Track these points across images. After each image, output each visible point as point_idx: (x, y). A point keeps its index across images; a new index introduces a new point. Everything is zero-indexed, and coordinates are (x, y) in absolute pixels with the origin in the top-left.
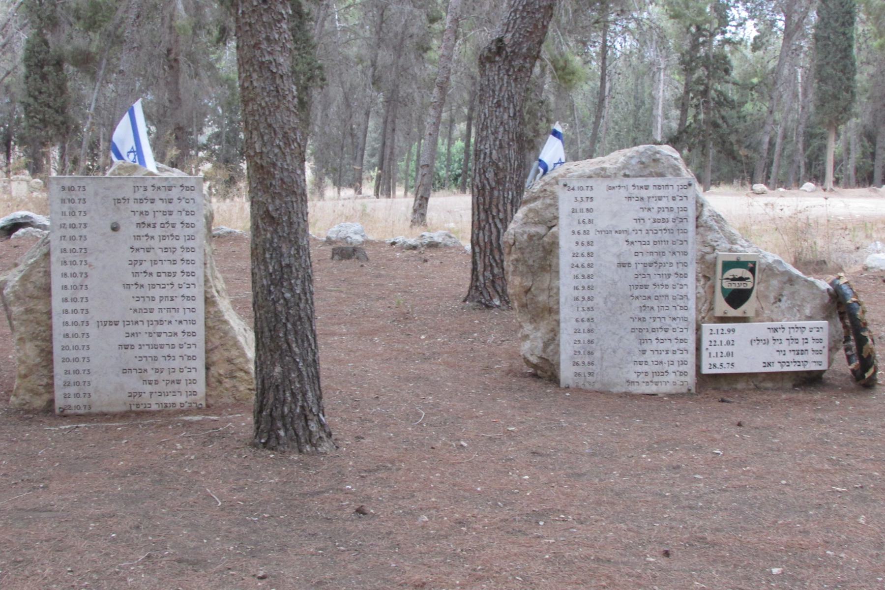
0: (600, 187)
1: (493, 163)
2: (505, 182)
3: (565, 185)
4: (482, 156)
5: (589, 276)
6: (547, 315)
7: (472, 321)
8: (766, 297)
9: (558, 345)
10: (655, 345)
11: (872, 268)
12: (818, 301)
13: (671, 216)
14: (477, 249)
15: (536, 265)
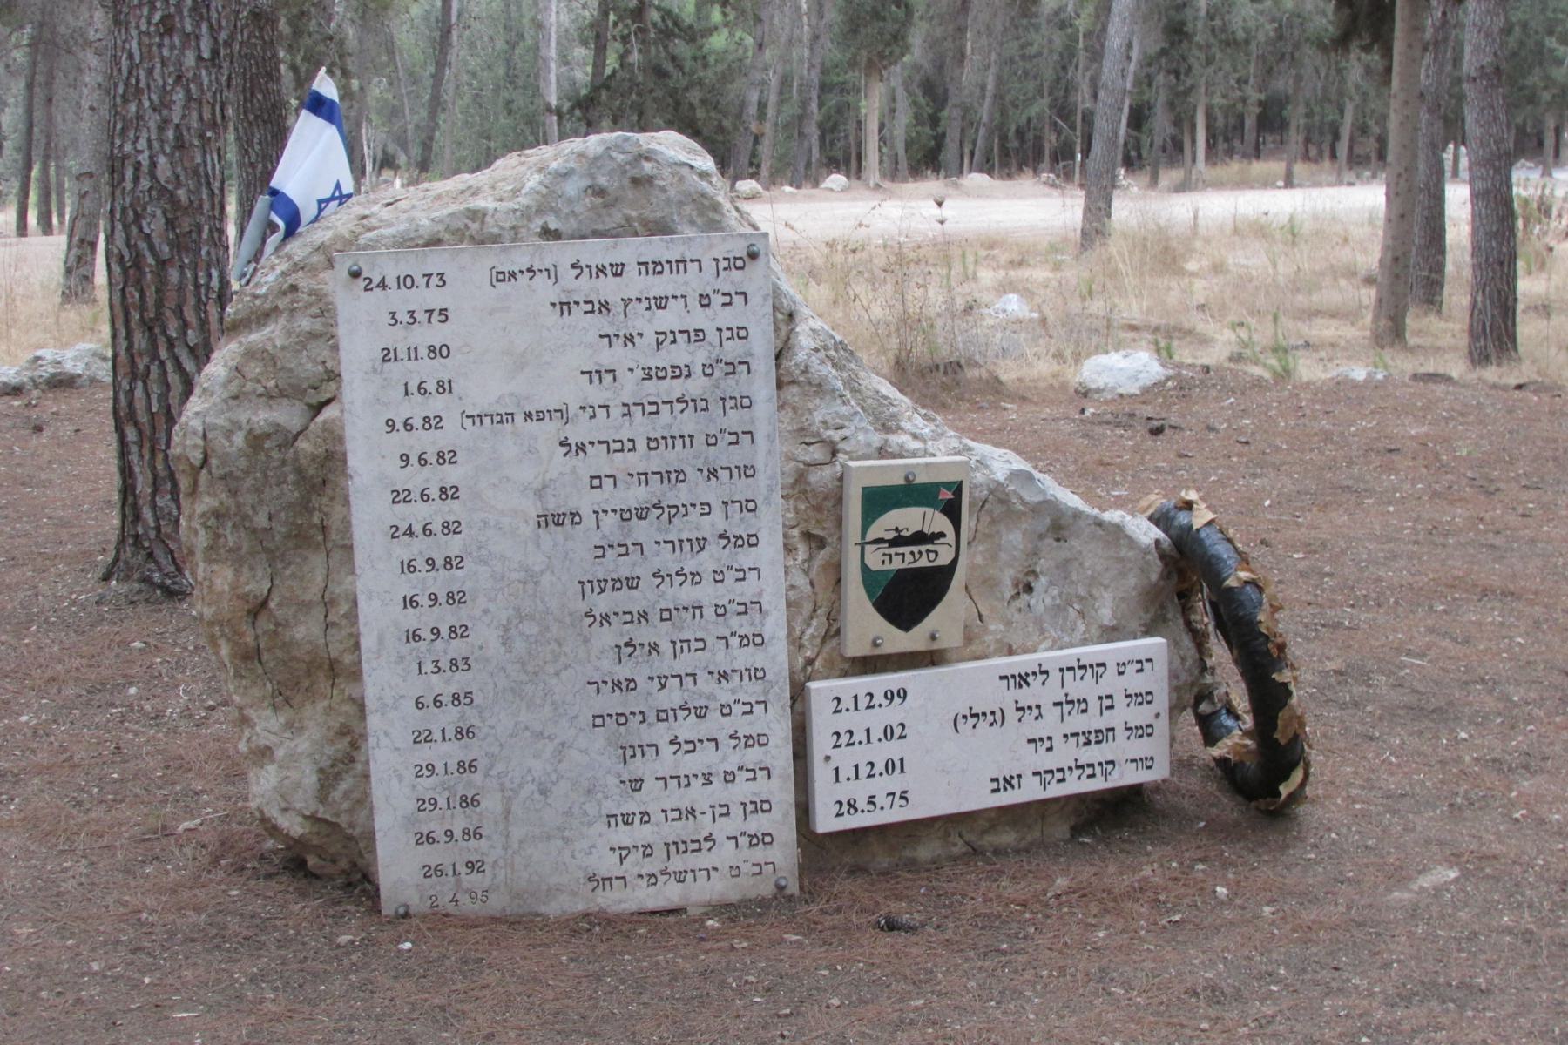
0: (469, 272)
1: (163, 190)
2: (198, 243)
3: (355, 275)
4: (129, 173)
5: (448, 562)
6: (323, 685)
7: (125, 644)
8: (990, 584)
9: (366, 776)
10: (668, 760)
11: (1098, 391)
12: (1132, 580)
13: (700, 356)
14: (131, 434)
15: (280, 529)
